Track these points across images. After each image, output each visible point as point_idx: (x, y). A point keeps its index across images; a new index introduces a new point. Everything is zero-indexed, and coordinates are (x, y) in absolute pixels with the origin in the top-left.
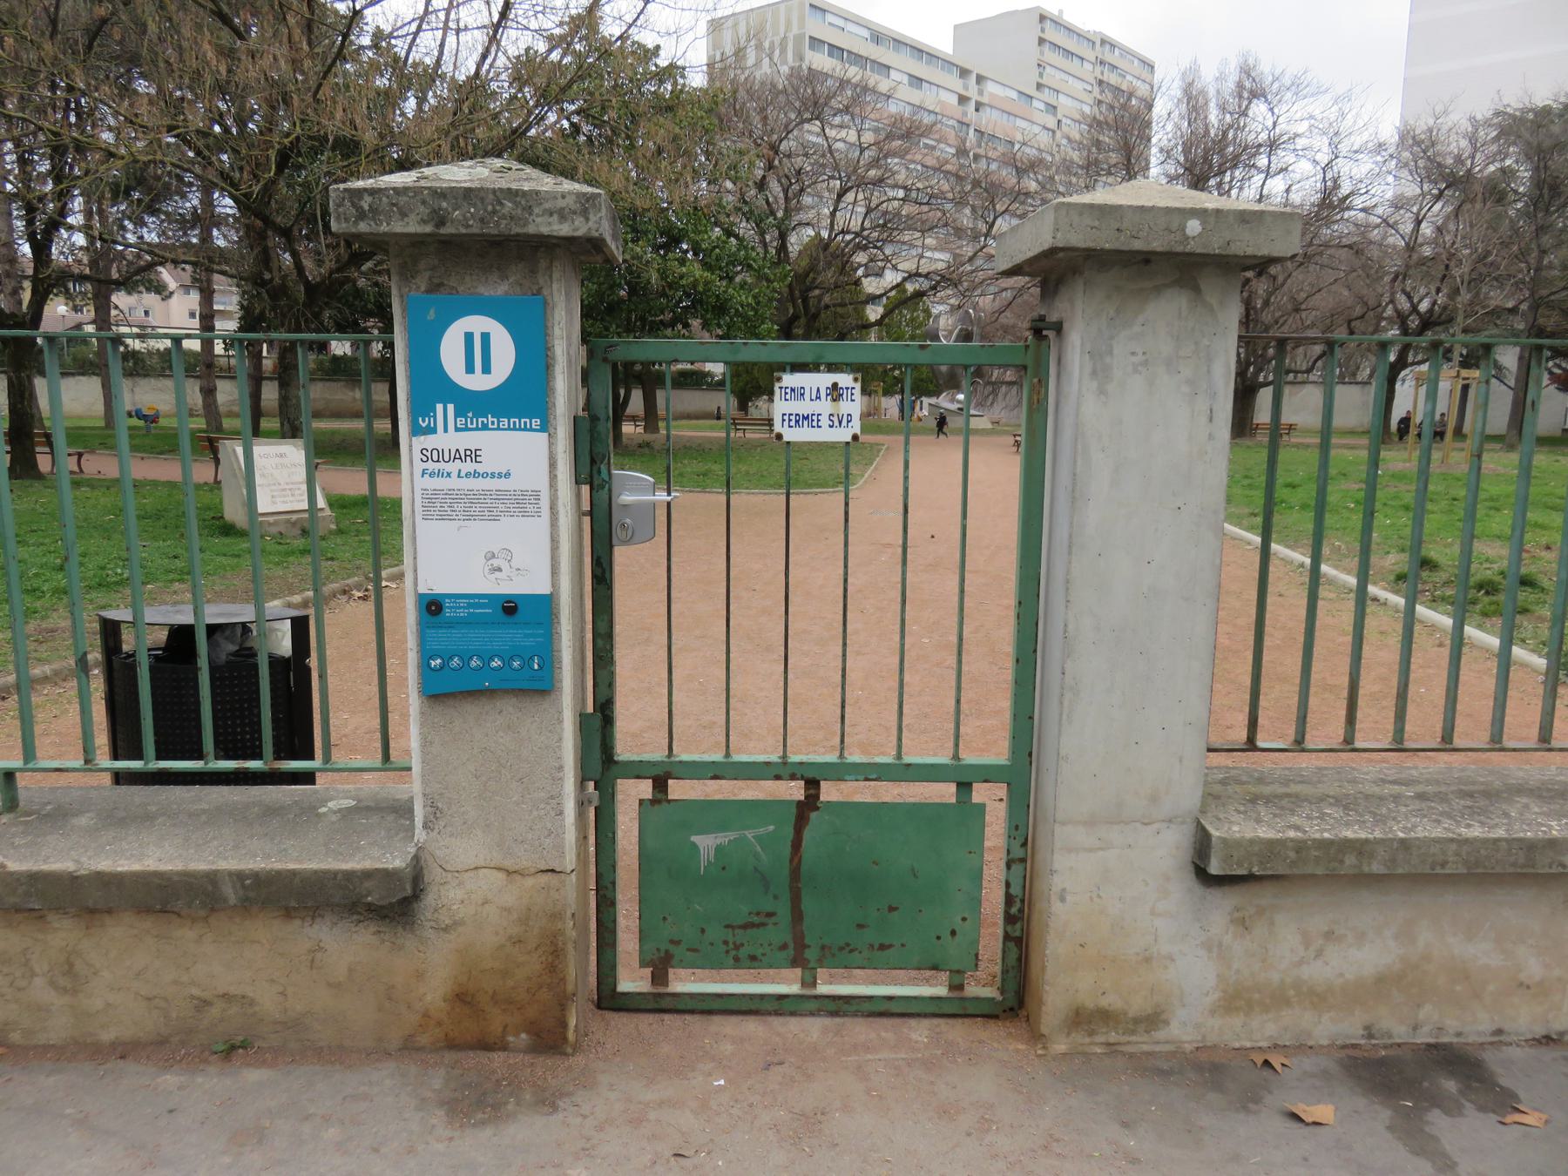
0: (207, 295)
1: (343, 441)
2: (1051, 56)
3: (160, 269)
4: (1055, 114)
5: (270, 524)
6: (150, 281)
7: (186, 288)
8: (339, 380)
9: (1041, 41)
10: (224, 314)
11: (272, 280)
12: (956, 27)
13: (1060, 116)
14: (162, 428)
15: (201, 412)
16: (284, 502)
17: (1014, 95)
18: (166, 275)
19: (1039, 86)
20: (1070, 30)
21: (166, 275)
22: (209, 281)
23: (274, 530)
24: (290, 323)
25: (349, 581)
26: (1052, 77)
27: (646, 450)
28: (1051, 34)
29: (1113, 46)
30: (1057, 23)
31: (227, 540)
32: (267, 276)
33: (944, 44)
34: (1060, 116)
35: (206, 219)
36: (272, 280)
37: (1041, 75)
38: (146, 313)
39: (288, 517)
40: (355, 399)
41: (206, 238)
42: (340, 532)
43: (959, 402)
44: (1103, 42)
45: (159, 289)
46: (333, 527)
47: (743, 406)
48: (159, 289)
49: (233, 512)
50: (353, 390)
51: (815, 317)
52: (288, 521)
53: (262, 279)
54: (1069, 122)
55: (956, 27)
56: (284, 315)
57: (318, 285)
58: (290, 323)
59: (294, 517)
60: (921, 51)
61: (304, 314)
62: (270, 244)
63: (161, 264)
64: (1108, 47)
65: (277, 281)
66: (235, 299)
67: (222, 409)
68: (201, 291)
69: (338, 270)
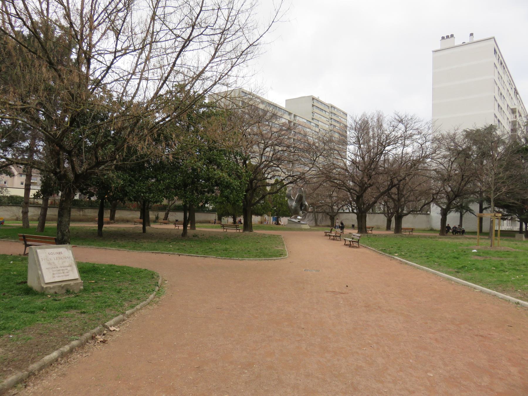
0: (29, 177)
1: (77, 233)
2: (316, 110)
3: (11, 167)
4: (318, 127)
5: (50, 288)
6: (7, 171)
7: (21, 174)
8: (75, 208)
9: (313, 106)
10: (35, 184)
11: (60, 172)
12: (286, 100)
13: (320, 128)
14: (5, 226)
15: (21, 219)
16: (59, 277)
17: (305, 121)
18: (13, 169)
19: (313, 119)
20: (322, 103)
21: (13, 169)
22: (31, 172)
23: (52, 291)
24: (66, 190)
25: (95, 330)
26: (316, 116)
27: (196, 238)
28: (316, 104)
29: (335, 108)
30: (318, 101)
31: (27, 298)
32: (58, 170)
33: (283, 105)
34: (320, 128)
35: (31, 150)
36: (60, 172)
37: (313, 116)
38: (5, 183)
39: (60, 284)
40: (80, 215)
41: (31, 156)
42: (85, 290)
43: (298, 219)
44: (332, 107)
45: (11, 175)
46: (82, 288)
47: (220, 219)
48: (11, 175)
49: (32, 282)
50: (80, 211)
51: (255, 189)
52: (60, 286)
53: (56, 172)
54: (322, 130)
55: (286, 100)
56: (64, 187)
57: (80, 174)
58: (66, 190)
59: (63, 284)
60: (277, 107)
61: (73, 187)
62: (61, 157)
63: (11, 164)
64: (333, 108)
65: (62, 172)
66: (39, 178)
67: (29, 218)
68: (27, 175)
69: (90, 169)
